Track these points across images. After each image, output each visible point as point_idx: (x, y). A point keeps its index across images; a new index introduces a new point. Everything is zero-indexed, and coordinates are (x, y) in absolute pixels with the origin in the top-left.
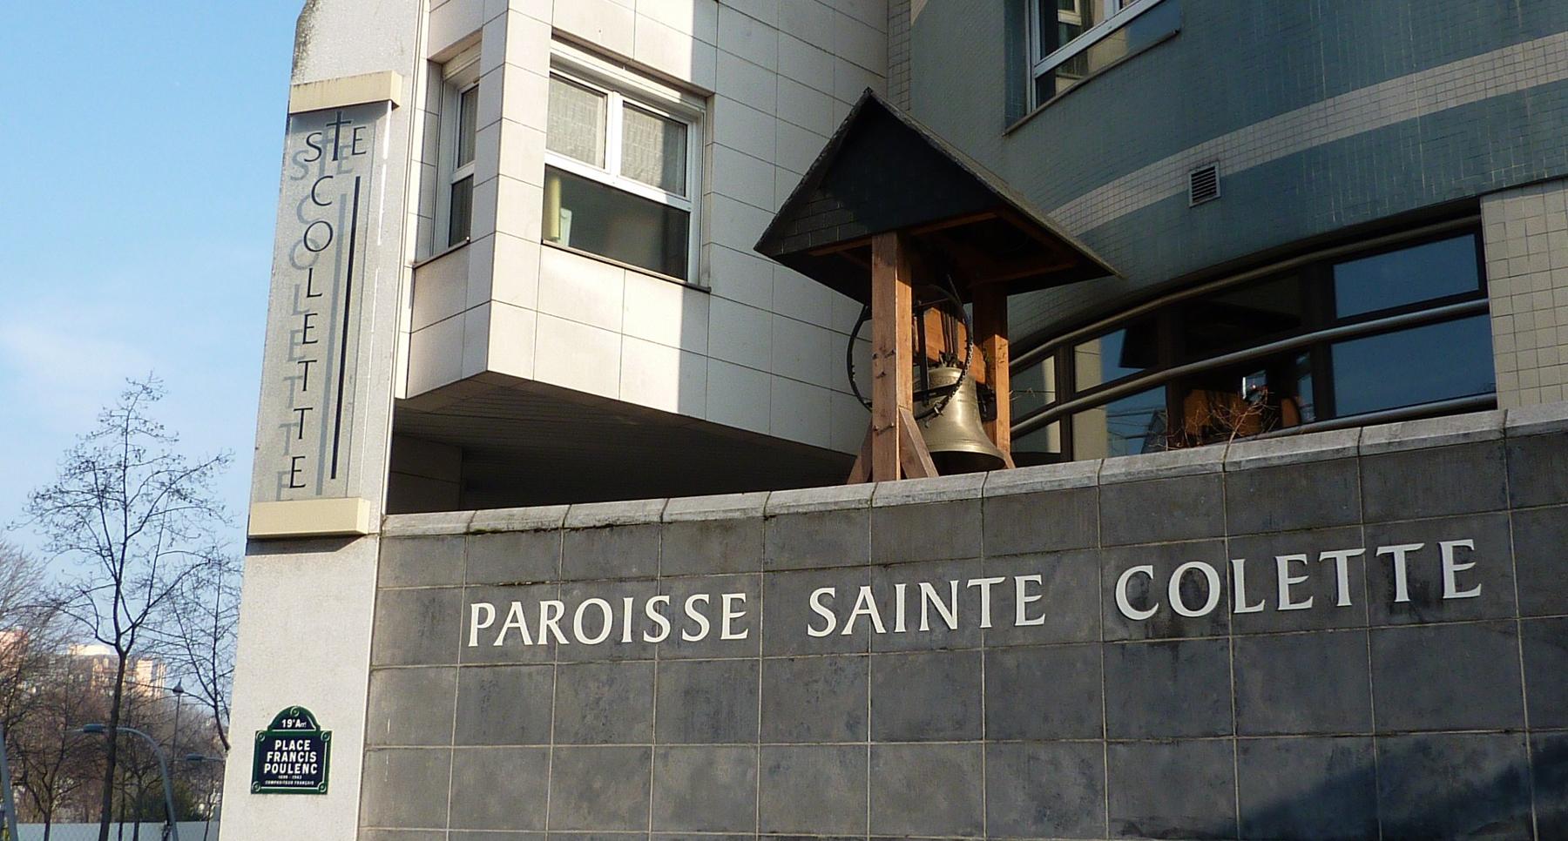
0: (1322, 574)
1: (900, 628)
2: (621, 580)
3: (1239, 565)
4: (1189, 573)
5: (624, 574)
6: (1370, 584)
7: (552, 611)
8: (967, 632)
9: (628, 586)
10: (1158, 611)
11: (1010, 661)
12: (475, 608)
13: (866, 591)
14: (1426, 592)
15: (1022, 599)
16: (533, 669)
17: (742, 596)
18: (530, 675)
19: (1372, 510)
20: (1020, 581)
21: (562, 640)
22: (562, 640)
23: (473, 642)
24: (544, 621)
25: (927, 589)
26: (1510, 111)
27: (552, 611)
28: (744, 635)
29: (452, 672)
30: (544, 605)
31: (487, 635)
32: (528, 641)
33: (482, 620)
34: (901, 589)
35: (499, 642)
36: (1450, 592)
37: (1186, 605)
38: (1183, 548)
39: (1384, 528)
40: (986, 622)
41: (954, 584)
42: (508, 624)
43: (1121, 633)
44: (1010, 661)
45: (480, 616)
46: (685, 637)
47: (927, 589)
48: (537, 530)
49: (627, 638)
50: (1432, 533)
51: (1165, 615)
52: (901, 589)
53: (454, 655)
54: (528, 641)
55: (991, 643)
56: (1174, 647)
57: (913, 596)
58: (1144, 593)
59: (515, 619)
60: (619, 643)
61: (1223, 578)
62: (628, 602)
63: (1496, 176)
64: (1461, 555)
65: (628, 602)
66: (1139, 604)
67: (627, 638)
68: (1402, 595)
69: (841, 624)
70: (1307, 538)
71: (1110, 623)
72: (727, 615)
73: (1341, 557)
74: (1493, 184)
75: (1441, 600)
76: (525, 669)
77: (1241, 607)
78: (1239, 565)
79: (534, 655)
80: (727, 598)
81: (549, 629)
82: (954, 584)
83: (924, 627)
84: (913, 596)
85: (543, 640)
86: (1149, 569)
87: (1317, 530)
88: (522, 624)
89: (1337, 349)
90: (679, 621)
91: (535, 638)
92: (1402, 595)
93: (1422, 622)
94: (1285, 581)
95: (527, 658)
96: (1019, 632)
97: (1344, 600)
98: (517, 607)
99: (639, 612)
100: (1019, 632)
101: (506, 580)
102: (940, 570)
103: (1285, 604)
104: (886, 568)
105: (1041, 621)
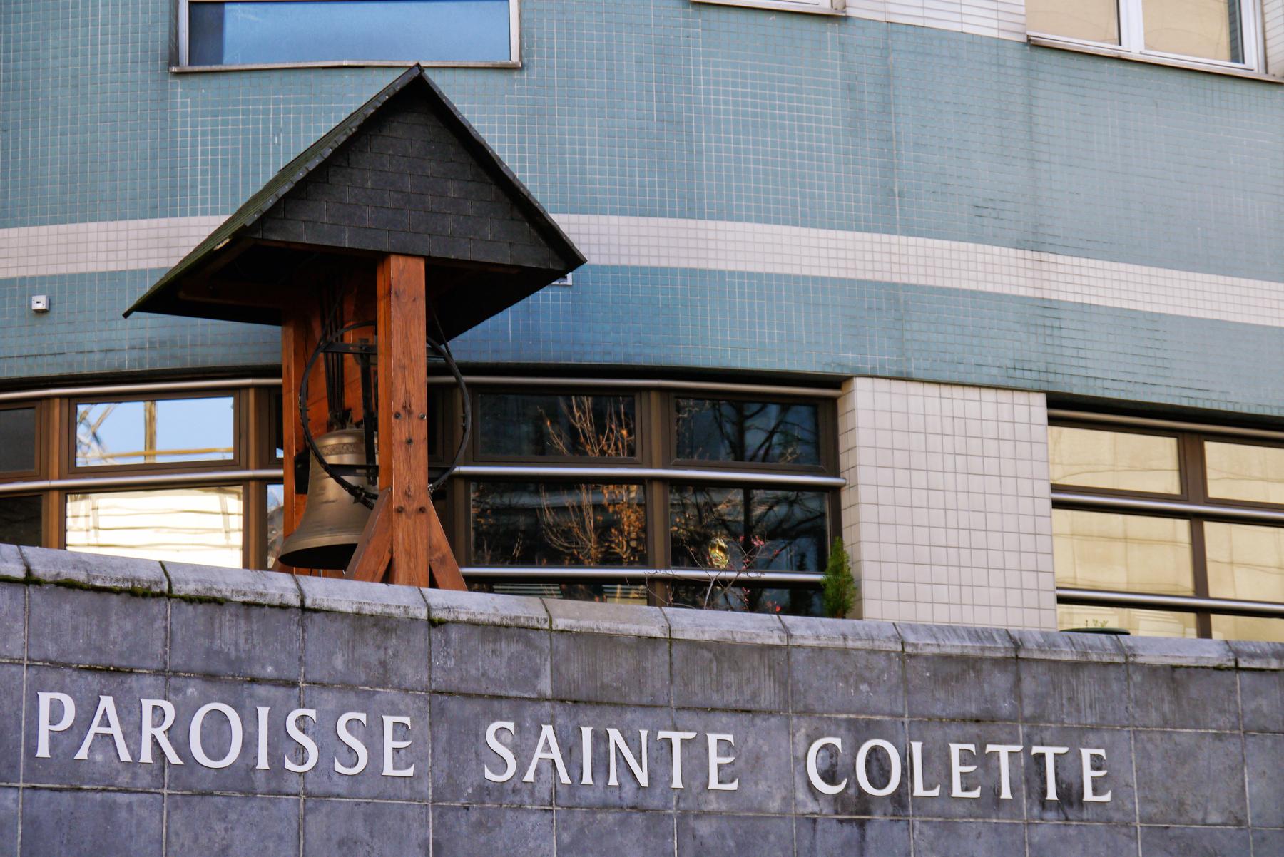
0: (987, 762)
1: (587, 779)
2: (253, 681)
3: (917, 747)
4: (874, 750)
5: (257, 671)
6: (1028, 781)
7: (158, 712)
8: (658, 791)
9: (261, 691)
10: (847, 787)
11: (704, 828)
12: (45, 699)
13: (548, 731)
14: (1070, 796)
15: (714, 760)
16: (134, 797)
17: (407, 720)
18: (129, 806)
19: (1028, 711)
20: (713, 739)
21: (174, 758)
22: (174, 758)
23: (43, 751)
24: (147, 730)
25: (615, 735)
26: (895, 302)
27: (158, 712)
28: (409, 772)
29: (12, 795)
30: (147, 705)
31: (66, 741)
32: (125, 756)
33: (55, 718)
34: (587, 732)
35: (82, 754)
36: (1088, 796)
37: (872, 782)
38: (868, 723)
39: (1036, 728)
40: (677, 783)
41: (644, 733)
42: (95, 728)
43: (812, 806)
44: (704, 828)
45: (54, 711)
46: (338, 767)
47: (615, 735)
48: (133, 593)
49: (263, 763)
50: (1074, 736)
51: (852, 791)
52: (587, 732)
53: (13, 767)
54: (125, 756)
55: (682, 805)
56: (862, 824)
57: (600, 739)
58: (834, 766)
59: (105, 722)
60: (253, 769)
61: (903, 759)
62: (263, 712)
63: (871, 360)
64: (1097, 763)
65: (263, 712)
66: (830, 776)
67: (263, 763)
68: (1052, 795)
69: (522, 770)
70: (973, 729)
71: (801, 794)
72: (389, 744)
73: (1003, 751)
74: (867, 368)
75: (1082, 803)
76: (122, 798)
77: (919, 790)
78: (917, 747)
79: (134, 776)
80: (389, 721)
81: (155, 743)
82: (644, 733)
83: (613, 781)
84: (600, 739)
85: (146, 756)
86: (837, 742)
87: (983, 723)
88: (116, 729)
89: (1191, 594)
90: (331, 746)
91: (135, 754)
92: (1052, 795)
93: (1067, 819)
94: (957, 769)
95: (124, 780)
96: (712, 797)
97: (1006, 793)
98: (107, 703)
99: (277, 728)
100: (712, 797)
101: (88, 661)
102: (629, 716)
103: (957, 791)
104: (573, 701)
105: (733, 786)
